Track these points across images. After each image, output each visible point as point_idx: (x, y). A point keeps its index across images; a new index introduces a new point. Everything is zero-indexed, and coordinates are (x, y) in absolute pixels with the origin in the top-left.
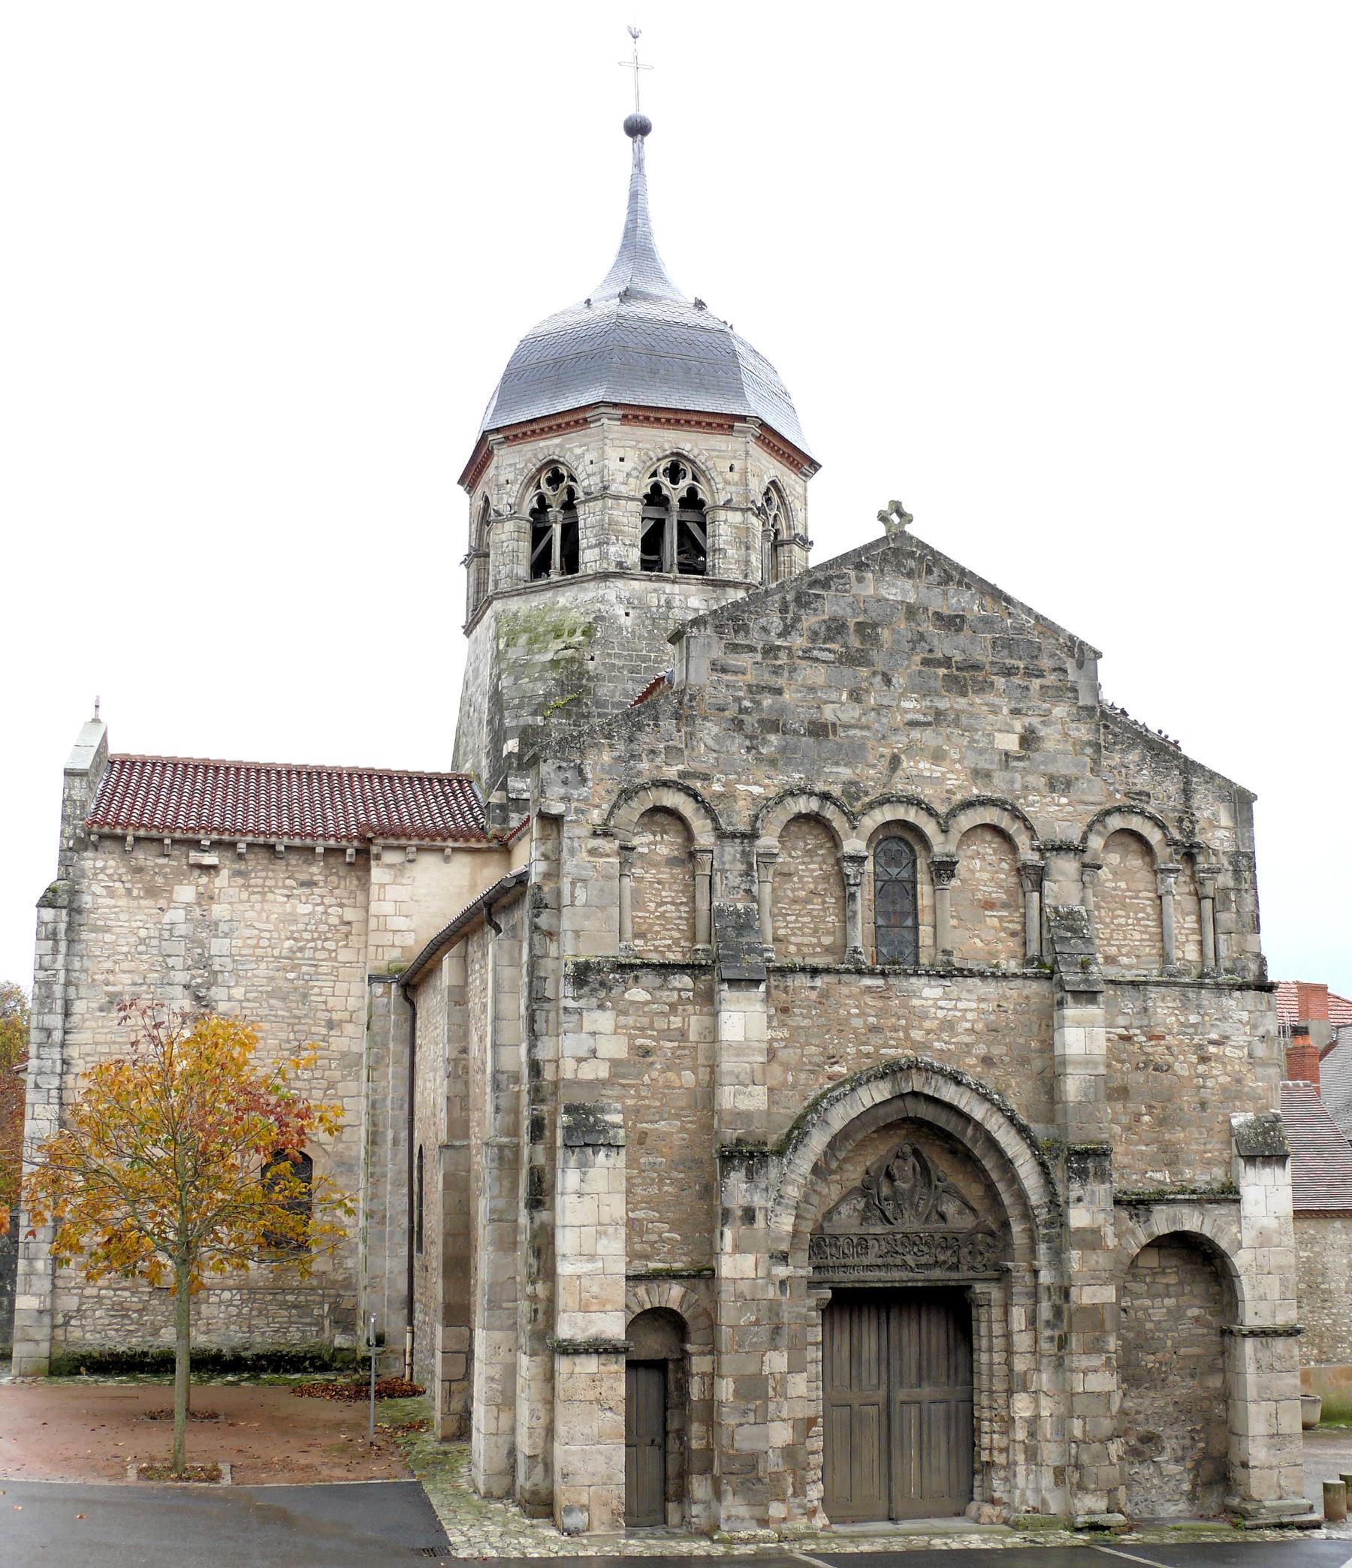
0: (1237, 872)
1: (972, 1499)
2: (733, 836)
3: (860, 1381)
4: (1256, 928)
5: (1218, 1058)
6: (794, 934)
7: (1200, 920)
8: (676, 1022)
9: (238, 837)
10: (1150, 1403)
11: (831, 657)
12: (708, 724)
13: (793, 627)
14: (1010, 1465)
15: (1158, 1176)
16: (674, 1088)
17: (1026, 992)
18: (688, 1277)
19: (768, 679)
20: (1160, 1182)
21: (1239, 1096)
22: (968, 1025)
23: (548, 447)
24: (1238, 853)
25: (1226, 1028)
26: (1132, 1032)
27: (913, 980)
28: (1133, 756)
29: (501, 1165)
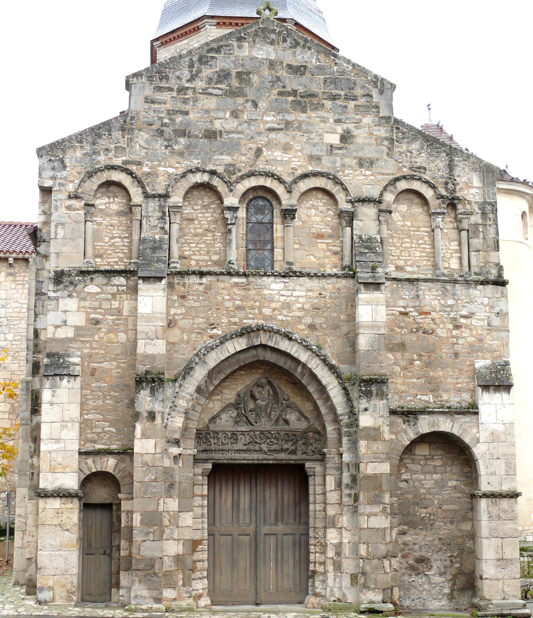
0: (484, 214)
1: (308, 594)
2: (154, 196)
3: (238, 520)
4: (497, 247)
5: (466, 326)
6: (195, 255)
7: (460, 245)
8: (115, 304)
9: (8, 255)
10: (417, 539)
11: (220, 92)
12: (142, 133)
13: (196, 76)
14: (325, 573)
15: (425, 398)
16: (113, 343)
17: (338, 286)
18: (119, 453)
19: (180, 106)
20: (426, 401)
21: (481, 349)
22: (300, 306)
23: (182, 45)
24: (485, 202)
25: (473, 308)
26: (408, 310)
27: (265, 279)
28: (415, 146)
29: (27, 392)
